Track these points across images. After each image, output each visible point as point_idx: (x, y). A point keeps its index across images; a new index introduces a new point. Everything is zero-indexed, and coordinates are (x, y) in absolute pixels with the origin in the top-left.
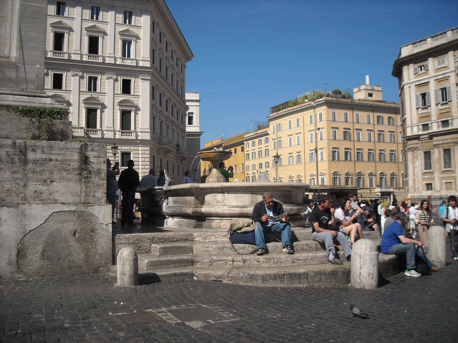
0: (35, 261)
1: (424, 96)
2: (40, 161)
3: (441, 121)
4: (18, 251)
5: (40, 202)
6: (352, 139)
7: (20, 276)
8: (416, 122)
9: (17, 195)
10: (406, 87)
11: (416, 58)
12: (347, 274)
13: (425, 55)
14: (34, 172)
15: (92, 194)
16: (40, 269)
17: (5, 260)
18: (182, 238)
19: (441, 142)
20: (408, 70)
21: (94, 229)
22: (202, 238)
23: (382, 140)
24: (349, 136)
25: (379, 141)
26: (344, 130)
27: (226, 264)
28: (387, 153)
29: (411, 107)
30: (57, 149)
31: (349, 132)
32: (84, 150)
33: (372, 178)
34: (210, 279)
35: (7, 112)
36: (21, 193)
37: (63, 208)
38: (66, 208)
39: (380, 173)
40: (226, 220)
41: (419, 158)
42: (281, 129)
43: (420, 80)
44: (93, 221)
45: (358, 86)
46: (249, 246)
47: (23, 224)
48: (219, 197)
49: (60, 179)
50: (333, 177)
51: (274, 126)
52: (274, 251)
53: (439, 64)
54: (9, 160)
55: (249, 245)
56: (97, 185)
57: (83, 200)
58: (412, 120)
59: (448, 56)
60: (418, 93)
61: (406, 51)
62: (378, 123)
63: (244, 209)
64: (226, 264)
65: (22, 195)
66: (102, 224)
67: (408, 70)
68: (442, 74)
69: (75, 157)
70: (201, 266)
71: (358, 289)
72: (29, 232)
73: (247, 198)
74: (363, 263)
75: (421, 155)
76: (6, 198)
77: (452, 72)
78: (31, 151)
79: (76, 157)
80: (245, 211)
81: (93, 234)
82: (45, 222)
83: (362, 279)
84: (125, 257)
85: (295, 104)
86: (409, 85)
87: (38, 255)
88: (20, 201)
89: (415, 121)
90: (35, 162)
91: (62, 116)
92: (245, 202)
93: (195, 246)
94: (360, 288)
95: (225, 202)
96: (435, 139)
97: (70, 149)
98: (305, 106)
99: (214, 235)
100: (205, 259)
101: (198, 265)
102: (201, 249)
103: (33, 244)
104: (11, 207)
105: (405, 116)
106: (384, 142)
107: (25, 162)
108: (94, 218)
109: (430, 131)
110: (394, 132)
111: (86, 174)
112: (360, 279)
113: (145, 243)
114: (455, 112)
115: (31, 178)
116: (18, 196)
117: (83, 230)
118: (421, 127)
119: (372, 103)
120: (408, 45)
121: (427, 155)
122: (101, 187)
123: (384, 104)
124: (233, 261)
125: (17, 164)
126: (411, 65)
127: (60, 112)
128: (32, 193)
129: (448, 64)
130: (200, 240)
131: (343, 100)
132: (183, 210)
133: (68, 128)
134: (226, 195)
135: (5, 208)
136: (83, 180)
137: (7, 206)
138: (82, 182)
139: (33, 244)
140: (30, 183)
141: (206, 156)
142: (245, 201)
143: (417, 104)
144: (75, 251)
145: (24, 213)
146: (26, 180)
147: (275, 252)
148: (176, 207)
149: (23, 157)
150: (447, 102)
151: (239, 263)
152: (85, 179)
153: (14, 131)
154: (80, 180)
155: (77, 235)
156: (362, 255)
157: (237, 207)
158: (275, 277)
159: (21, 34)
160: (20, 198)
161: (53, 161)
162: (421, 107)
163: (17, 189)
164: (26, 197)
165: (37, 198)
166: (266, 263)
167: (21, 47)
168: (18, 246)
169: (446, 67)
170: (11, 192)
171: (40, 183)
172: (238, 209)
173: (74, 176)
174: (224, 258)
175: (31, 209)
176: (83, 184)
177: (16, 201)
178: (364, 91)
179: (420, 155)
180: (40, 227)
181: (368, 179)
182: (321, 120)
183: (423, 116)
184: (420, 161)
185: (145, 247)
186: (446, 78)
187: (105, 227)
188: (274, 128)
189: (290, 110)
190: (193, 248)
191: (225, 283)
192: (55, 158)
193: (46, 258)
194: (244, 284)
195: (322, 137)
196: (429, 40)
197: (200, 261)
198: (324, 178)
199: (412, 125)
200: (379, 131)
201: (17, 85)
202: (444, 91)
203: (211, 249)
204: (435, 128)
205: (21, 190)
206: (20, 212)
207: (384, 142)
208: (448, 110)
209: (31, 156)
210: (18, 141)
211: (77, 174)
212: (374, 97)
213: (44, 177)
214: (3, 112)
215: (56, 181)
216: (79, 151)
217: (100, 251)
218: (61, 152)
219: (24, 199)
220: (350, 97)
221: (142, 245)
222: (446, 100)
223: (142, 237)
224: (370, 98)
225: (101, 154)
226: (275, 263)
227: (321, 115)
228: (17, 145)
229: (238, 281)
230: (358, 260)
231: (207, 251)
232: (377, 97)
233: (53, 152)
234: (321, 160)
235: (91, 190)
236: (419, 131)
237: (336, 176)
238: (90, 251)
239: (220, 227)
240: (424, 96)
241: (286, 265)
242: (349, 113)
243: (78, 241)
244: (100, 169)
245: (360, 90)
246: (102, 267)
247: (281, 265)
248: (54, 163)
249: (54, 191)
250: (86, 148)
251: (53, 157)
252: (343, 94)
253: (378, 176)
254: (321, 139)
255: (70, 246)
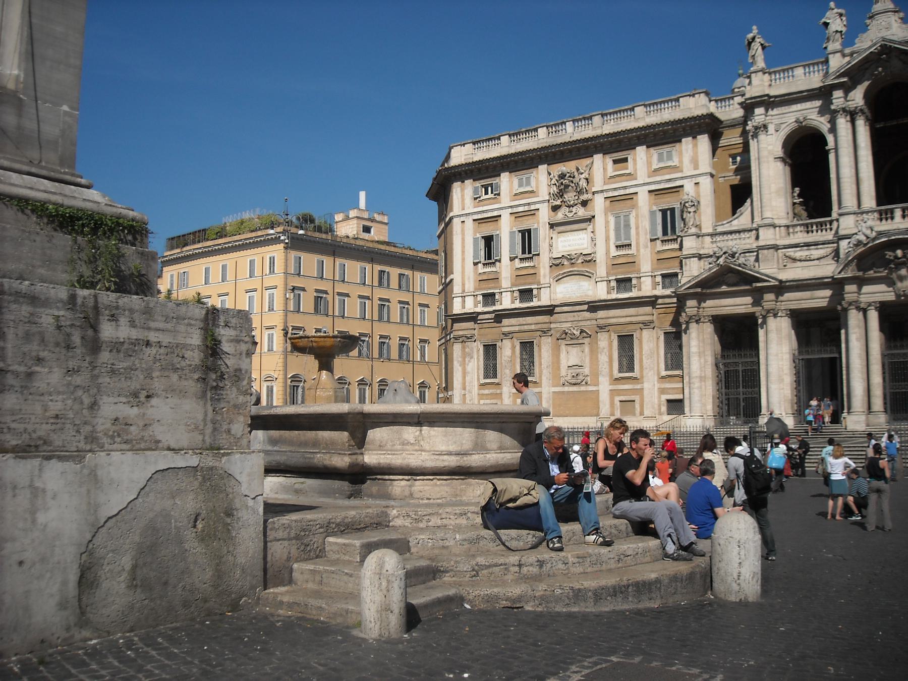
0: (117, 593)
1: (489, 241)
2: (126, 346)
3: (518, 290)
4: (81, 571)
5: (124, 446)
6: (330, 313)
7: (86, 633)
8: (472, 290)
9: (75, 428)
10: (456, 222)
11: (479, 170)
12: (708, 578)
13: (495, 166)
14: (113, 372)
15: (225, 427)
16: (126, 613)
17: (52, 596)
18: (372, 521)
19: (517, 329)
20: (462, 190)
21: (231, 509)
22: (409, 520)
23: (386, 319)
24: (325, 305)
25: (380, 319)
26: (315, 294)
27: (506, 572)
28: (394, 344)
29: (463, 259)
30: (160, 318)
31: (325, 298)
32: (211, 322)
33: (364, 389)
34: (498, 605)
35: (20, 214)
36: (85, 423)
37: (174, 462)
38: (180, 461)
39: (380, 381)
40: (423, 480)
41: (475, 357)
42: (187, 283)
43: (483, 212)
44: (231, 491)
45: (345, 210)
46: (528, 534)
47: (92, 502)
48: (410, 433)
49: (165, 390)
50: (290, 386)
51: (172, 276)
52: (569, 540)
53: (520, 185)
54: (61, 338)
55: (528, 531)
56: (236, 406)
57: (208, 440)
58: (463, 285)
59: (537, 173)
60: (478, 235)
61: (460, 156)
62: (380, 284)
63: (465, 458)
64: (506, 572)
65: (88, 428)
66: (246, 496)
67: (462, 190)
68: (524, 205)
69: (194, 340)
70: (454, 579)
71: (736, 602)
72: (106, 522)
73: (467, 435)
74: (745, 555)
75: (478, 350)
76: (54, 437)
77: (543, 202)
78: (107, 318)
79: (196, 339)
80: (466, 462)
81: (229, 520)
82: (138, 495)
83: (743, 585)
84: (390, 572)
85: (221, 234)
86: (462, 219)
87: (122, 578)
88: (82, 445)
89: (470, 286)
90: (116, 346)
91: (135, 239)
92: (462, 444)
93: (414, 537)
94: (738, 600)
95: (422, 443)
96: (505, 321)
97: (185, 319)
98: (241, 240)
99: (437, 514)
100: (462, 565)
101: (445, 579)
102: (430, 544)
103: (113, 551)
104: (68, 461)
105: (451, 277)
106: (388, 321)
107: (94, 346)
108: (233, 482)
109: (498, 307)
110: (408, 303)
111: (214, 381)
112: (739, 584)
113: (316, 536)
114: (545, 276)
115: (106, 387)
116: (78, 431)
117: (212, 511)
118: (480, 298)
119: (371, 245)
120: (464, 145)
121: (490, 351)
122: (241, 411)
123: (392, 249)
124: (520, 566)
125: (78, 351)
126: (468, 182)
127: (132, 226)
128: (108, 425)
129: (537, 187)
130: (406, 524)
131: (317, 235)
132: (315, 461)
133: (151, 266)
134: (425, 429)
135: (53, 461)
136: (209, 395)
137: (60, 458)
138: (206, 400)
139: (113, 551)
140: (105, 397)
141: (314, 344)
142: (464, 442)
143: (476, 255)
144: (195, 563)
145: (95, 475)
146: (95, 390)
147: (571, 542)
148: (286, 452)
149: (90, 332)
150: (531, 255)
151: (531, 569)
152: (213, 392)
153: (39, 263)
154: (203, 395)
155: (200, 526)
156: (742, 541)
157: (450, 454)
158: (617, 591)
159: (30, 23)
160: (82, 438)
161: (151, 346)
162: (483, 260)
163: (77, 413)
164: (94, 435)
165: (119, 435)
166: (578, 565)
167: (31, 55)
168: (80, 560)
169: (532, 192)
170: (63, 420)
171: (124, 400)
172: (453, 458)
173: (191, 385)
174: (502, 561)
175: (110, 464)
176: (209, 403)
177: (75, 444)
178: (355, 221)
179: (477, 350)
180: (129, 509)
181: (357, 391)
182: (272, 271)
183: (485, 277)
184: (476, 362)
185: (315, 545)
186: (533, 212)
187: (251, 503)
188: (172, 280)
189: (210, 246)
190: (409, 541)
191: (529, 612)
192: (156, 340)
193: (139, 584)
194: (564, 610)
195: (273, 305)
196: (505, 139)
197: (452, 570)
198: (272, 387)
199: (465, 294)
200: (380, 299)
201: (18, 148)
202: (527, 236)
203: (451, 543)
204: (507, 302)
205: (85, 417)
206: (86, 471)
207: (388, 321)
208: (532, 271)
209: (107, 331)
210: (81, 293)
211: (197, 379)
212: (374, 235)
213: (134, 385)
214: (10, 213)
215: (158, 396)
216: (202, 326)
217: (241, 560)
218: (169, 326)
219: (92, 438)
220: (331, 230)
221: (311, 540)
222: (530, 252)
223: (311, 523)
224: (366, 236)
225: (241, 335)
226: (592, 564)
227: (272, 260)
228: (79, 301)
229: (551, 605)
230: (735, 550)
231: (444, 547)
232: (378, 234)
233: (152, 325)
234: (268, 351)
235: (223, 417)
236: (476, 306)
237: (296, 384)
238: (224, 559)
239: (411, 494)
240: (489, 241)
241: (609, 567)
242: (328, 261)
243: (203, 540)
244: (240, 370)
245: (347, 218)
246: (246, 596)
247: (602, 569)
248: (153, 351)
249: (153, 420)
250: (214, 320)
251: (153, 337)
252: (317, 222)
253: (376, 387)
254: (271, 309)
255: (186, 550)
